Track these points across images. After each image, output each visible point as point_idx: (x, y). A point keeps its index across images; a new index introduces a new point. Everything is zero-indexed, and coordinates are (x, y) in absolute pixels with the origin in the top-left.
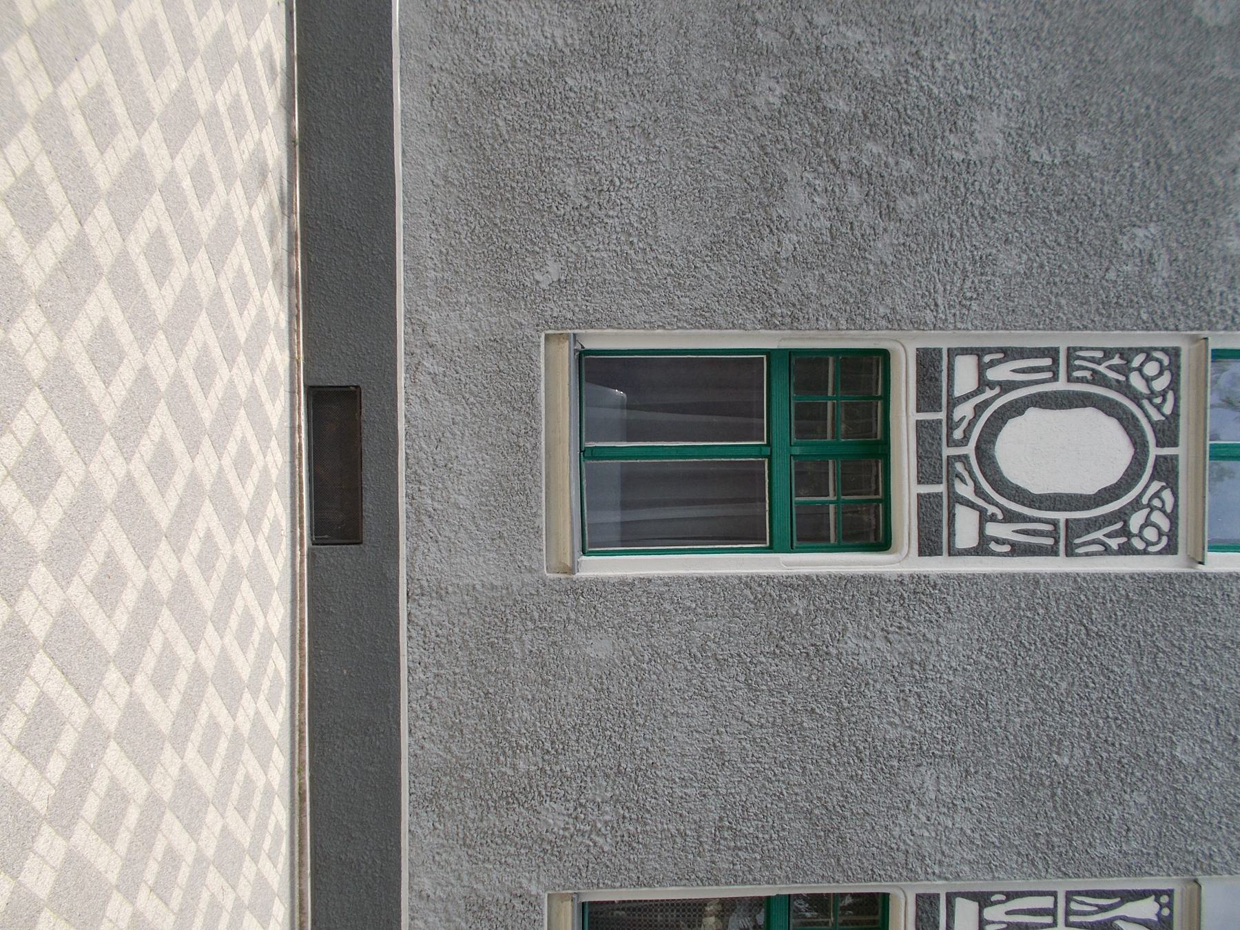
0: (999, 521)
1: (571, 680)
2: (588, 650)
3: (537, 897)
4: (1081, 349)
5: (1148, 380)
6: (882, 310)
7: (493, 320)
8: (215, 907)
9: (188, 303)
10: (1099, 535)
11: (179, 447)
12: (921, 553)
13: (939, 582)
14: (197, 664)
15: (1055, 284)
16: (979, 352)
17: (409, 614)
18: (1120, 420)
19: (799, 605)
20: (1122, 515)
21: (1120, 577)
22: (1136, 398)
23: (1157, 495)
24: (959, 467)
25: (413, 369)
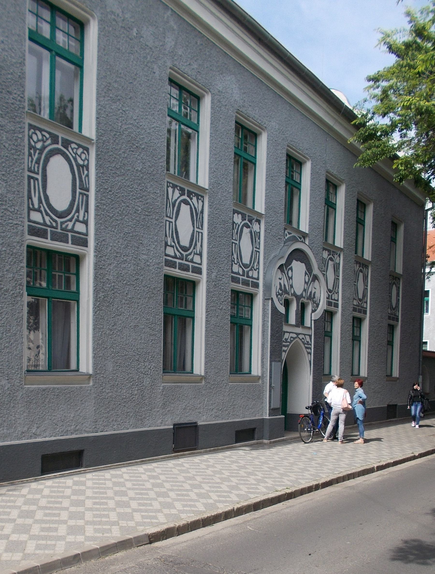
0: (79, 214)
1: (117, 376)
2: (111, 370)
3: (163, 387)
4: (28, 166)
5: (39, 140)
6: (18, 248)
7: (20, 406)
10: (83, 177)
12: (87, 246)
13: (97, 242)
15: (9, 171)
16: (29, 209)
17: (101, 432)
18: (51, 156)
19: (101, 295)
20: (78, 165)
21: (97, 174)
22: (44, 148)
23: (72, 150)
24: (64, 226)
25: (36, 435)
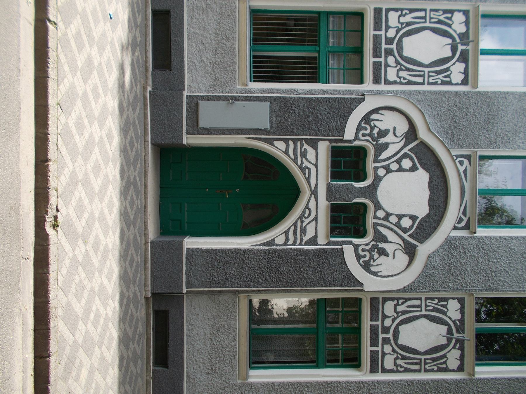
8: (98, 387)
9: (90, 144)
11: (86, 201)
14: (92, 288)
